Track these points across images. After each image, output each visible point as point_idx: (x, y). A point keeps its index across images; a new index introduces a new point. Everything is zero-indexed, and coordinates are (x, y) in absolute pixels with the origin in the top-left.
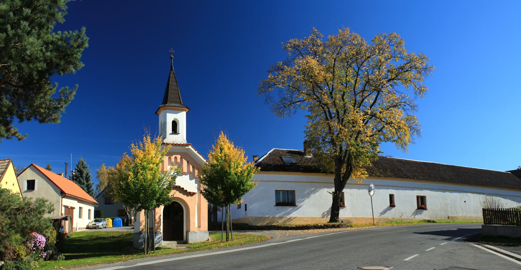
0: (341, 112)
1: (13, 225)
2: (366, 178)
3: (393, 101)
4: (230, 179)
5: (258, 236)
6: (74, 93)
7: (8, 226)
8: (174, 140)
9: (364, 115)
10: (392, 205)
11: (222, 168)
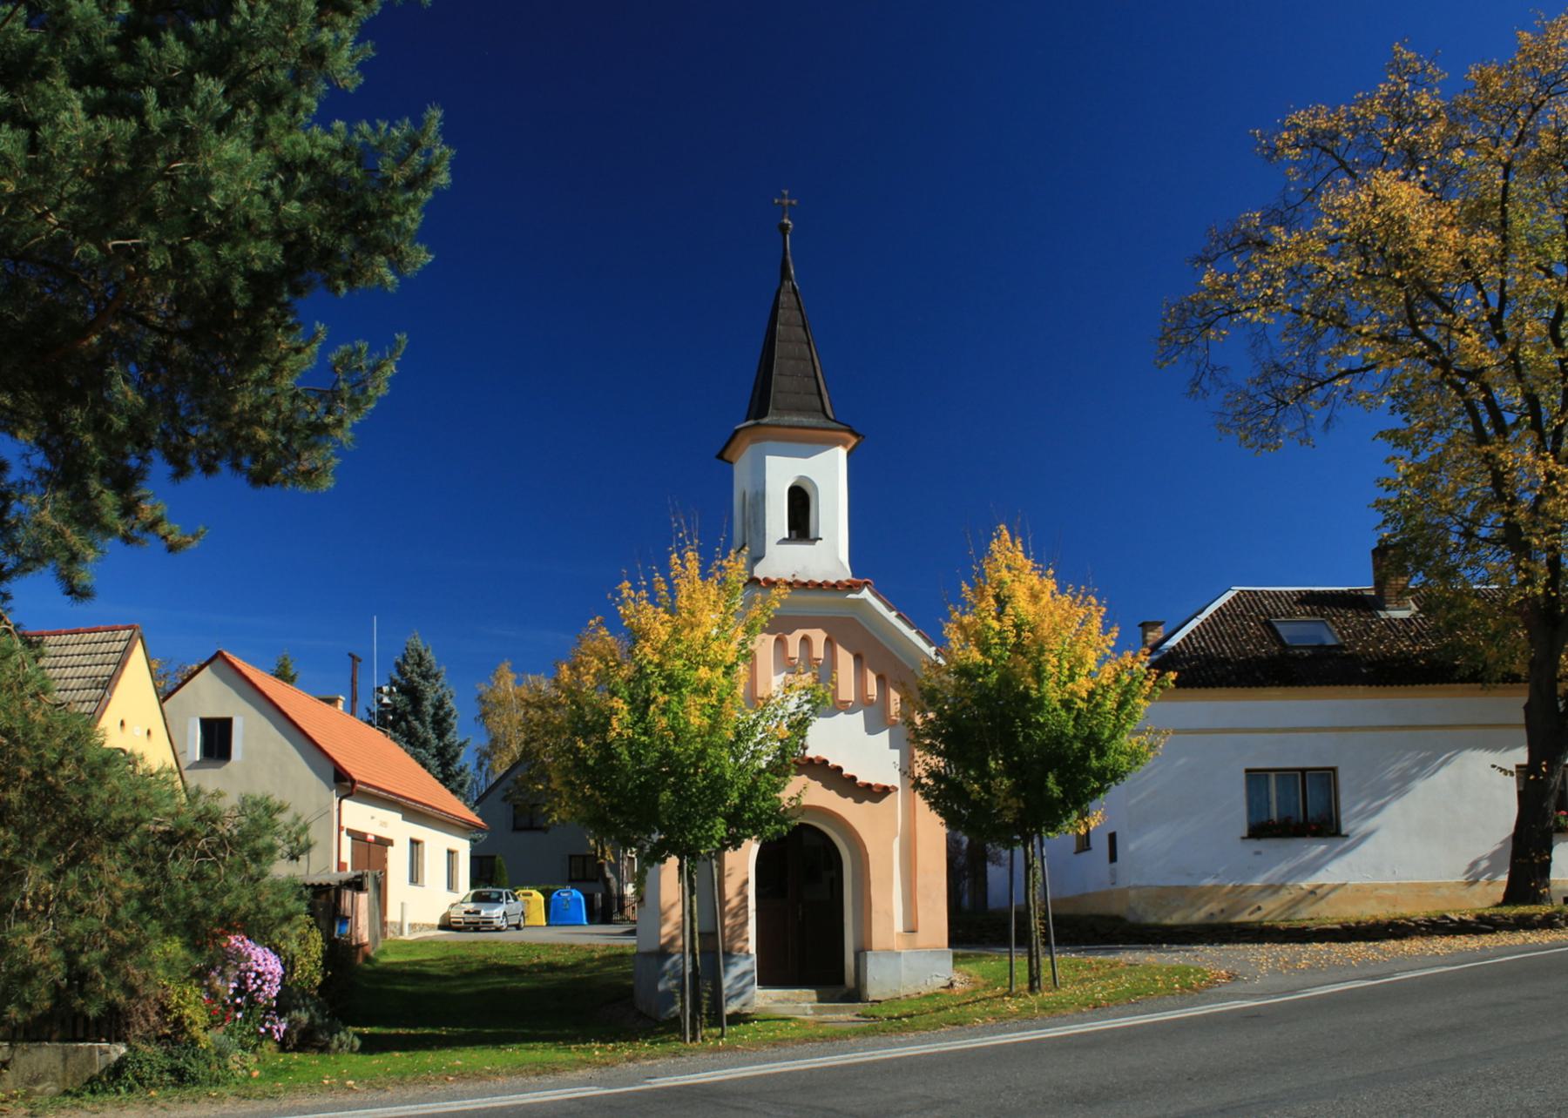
1: (154, 901)
4: (1040, 726)
5: (1172, 971)
6: (390, 369)
7: (135, 904)
11: (1007, 681)
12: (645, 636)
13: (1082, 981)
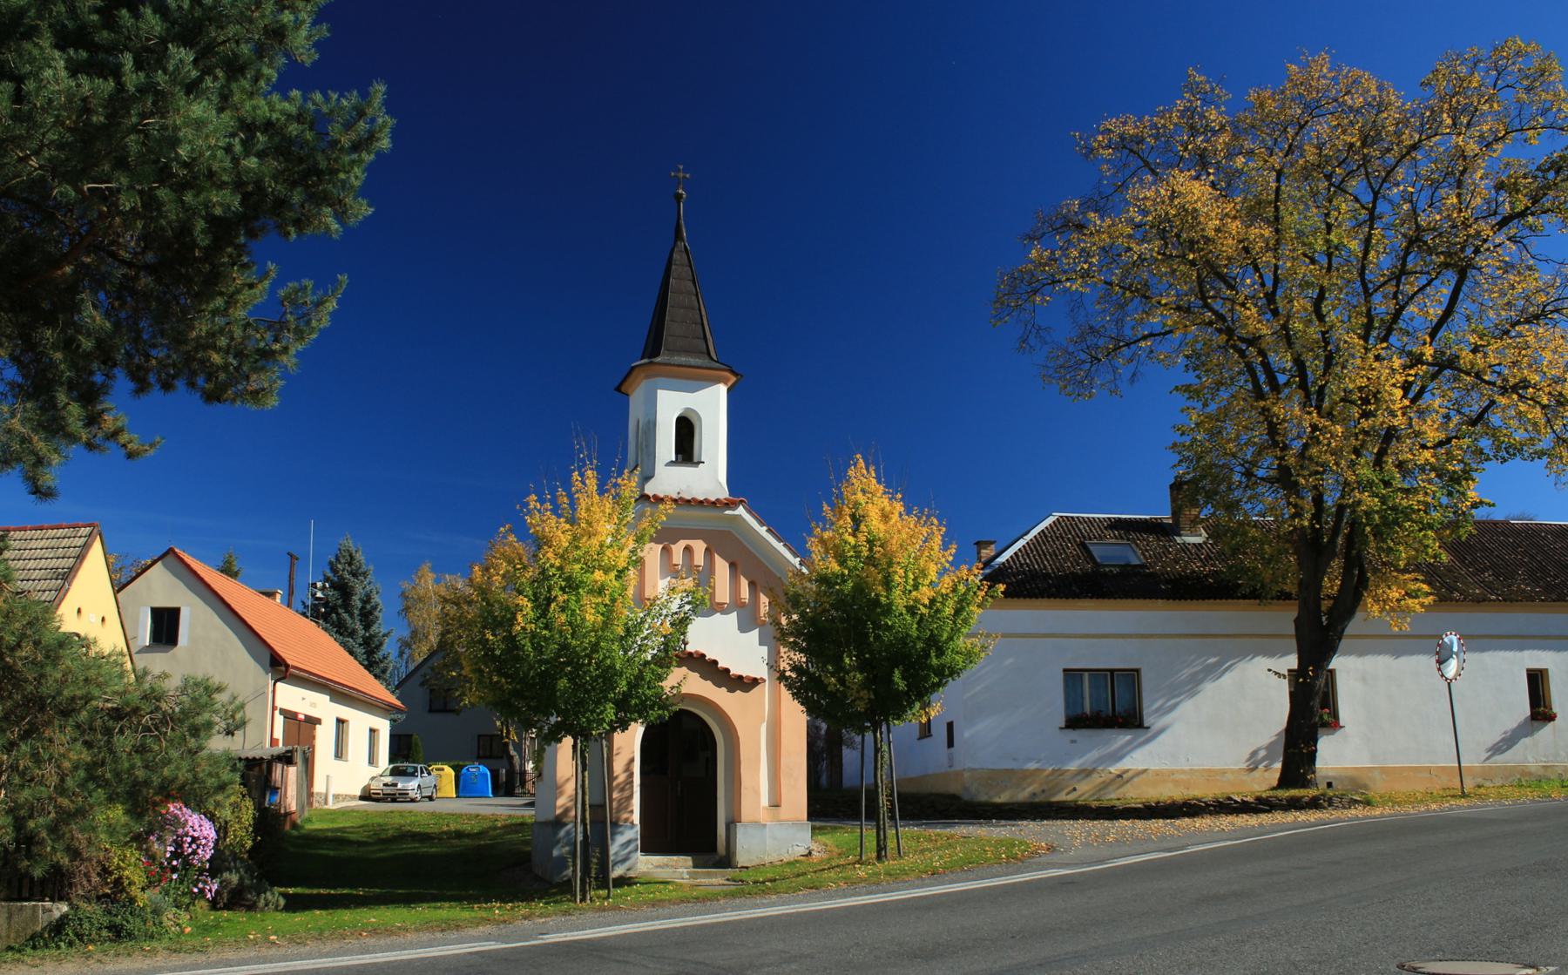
0: (1314, 365)
2: (1427, 607)
3: (1527, 299)
4: (889, 628)
5: (999, 842)
6: (332, 305)
7: (82, 773)
8: (684, 487)
9: (1405, 367)
10: (1541, 711)
11: (860, 589)
12: (549, 543)
13: (922, 851)
